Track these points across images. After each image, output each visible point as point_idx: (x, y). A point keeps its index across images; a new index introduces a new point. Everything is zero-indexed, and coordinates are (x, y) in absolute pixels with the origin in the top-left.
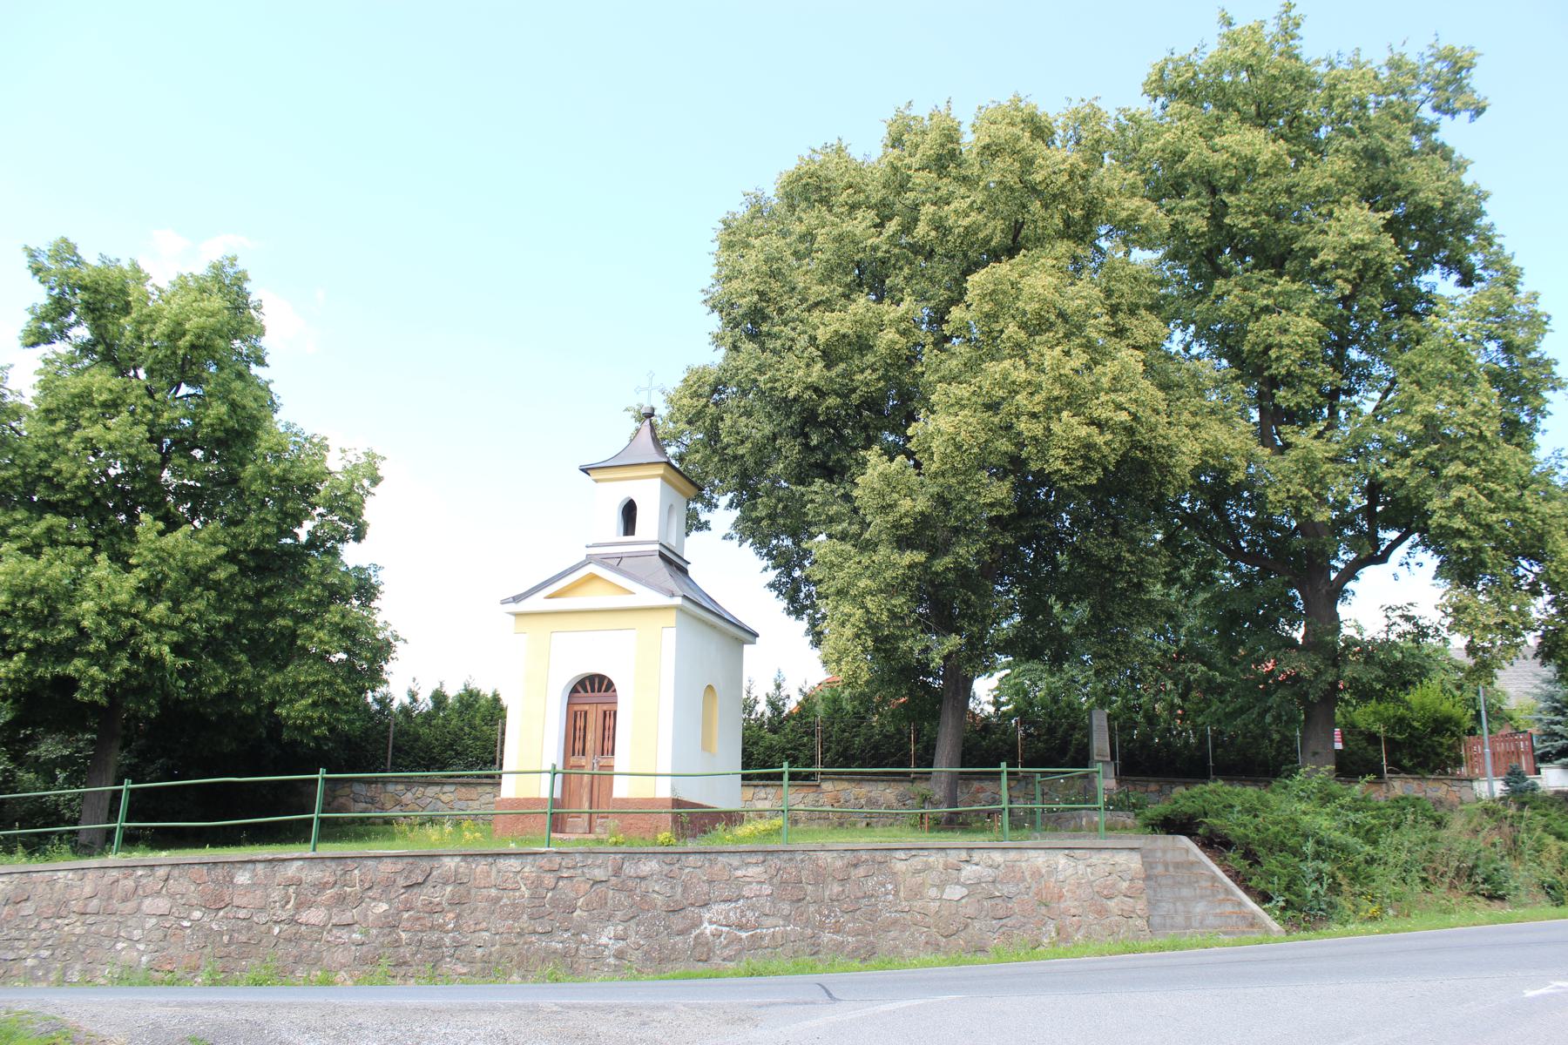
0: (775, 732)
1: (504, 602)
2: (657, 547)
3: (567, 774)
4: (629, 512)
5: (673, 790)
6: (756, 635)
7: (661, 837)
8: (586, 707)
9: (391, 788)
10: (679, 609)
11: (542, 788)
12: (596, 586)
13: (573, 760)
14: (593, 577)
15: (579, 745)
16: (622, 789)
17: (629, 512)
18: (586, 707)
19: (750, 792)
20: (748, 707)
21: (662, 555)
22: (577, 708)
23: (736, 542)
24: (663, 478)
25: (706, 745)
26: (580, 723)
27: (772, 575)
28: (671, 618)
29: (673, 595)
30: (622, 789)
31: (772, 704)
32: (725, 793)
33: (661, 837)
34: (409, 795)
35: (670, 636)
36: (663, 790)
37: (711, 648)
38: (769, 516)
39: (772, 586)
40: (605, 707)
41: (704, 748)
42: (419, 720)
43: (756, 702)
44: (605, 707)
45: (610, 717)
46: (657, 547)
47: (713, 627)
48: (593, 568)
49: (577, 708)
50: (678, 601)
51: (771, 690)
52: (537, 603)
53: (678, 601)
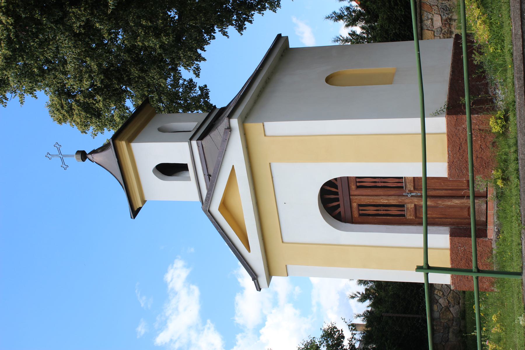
0: (377, 17)
1: (259, 289)
2: (194, 143)
3: (427, 221)
4: (168, 170)
5: (437, 114)
6: (279, 36)
7: (496, 129)
8: (355, 205)
9: (436, 315)
10: (243, 122)
11: (441, 240)
12: (232, 202)
13: (410, 216)
14: (224, 206)
15: (394, 211)
16: (439, 169)
17: (168, 170)
18: (355, 205)
19: (427, 33)
20: (355, 38)
21: (201, 138)
22: (356, 214)
23: (202, 64)
24: (130, 140)
25: (387, 79)
26: (371, 210)
27: (231, 30)
28: (254, 127)
29: (229, 129)
30: (439, 169)
31: (352, 22)
32: (438, 54)
33: (496, 129)
34: (441, 301)
35: (276, 128)
36: (438, 125)
37: (290, 80)
38: (157, 36)
39: (240, 28)
40: (353, 187)
41: (390, 82)
42: (383, 294)
43: (353, 34)
44: (353, 187)
45: (361, 183)
46: (194, 143)
47: (267, 81)
48: (215, 208)
49: (356, 214)
50: (235, 122)
51: (342, 23)
52: (255, 257)
53: (235, 122)
